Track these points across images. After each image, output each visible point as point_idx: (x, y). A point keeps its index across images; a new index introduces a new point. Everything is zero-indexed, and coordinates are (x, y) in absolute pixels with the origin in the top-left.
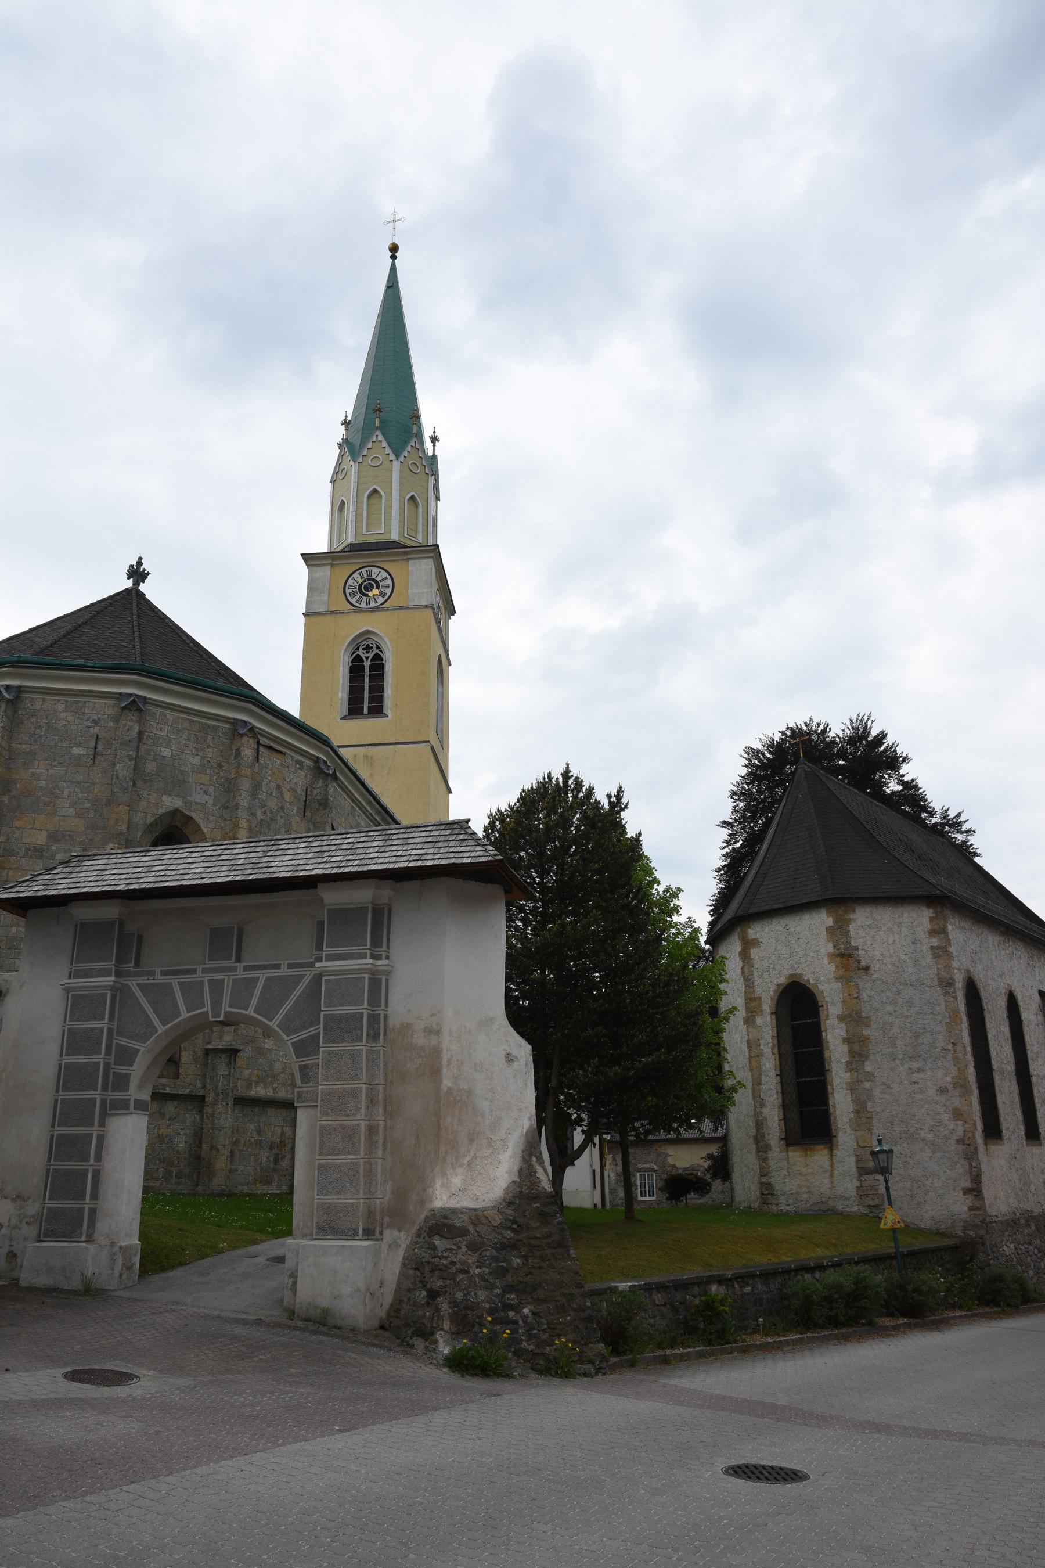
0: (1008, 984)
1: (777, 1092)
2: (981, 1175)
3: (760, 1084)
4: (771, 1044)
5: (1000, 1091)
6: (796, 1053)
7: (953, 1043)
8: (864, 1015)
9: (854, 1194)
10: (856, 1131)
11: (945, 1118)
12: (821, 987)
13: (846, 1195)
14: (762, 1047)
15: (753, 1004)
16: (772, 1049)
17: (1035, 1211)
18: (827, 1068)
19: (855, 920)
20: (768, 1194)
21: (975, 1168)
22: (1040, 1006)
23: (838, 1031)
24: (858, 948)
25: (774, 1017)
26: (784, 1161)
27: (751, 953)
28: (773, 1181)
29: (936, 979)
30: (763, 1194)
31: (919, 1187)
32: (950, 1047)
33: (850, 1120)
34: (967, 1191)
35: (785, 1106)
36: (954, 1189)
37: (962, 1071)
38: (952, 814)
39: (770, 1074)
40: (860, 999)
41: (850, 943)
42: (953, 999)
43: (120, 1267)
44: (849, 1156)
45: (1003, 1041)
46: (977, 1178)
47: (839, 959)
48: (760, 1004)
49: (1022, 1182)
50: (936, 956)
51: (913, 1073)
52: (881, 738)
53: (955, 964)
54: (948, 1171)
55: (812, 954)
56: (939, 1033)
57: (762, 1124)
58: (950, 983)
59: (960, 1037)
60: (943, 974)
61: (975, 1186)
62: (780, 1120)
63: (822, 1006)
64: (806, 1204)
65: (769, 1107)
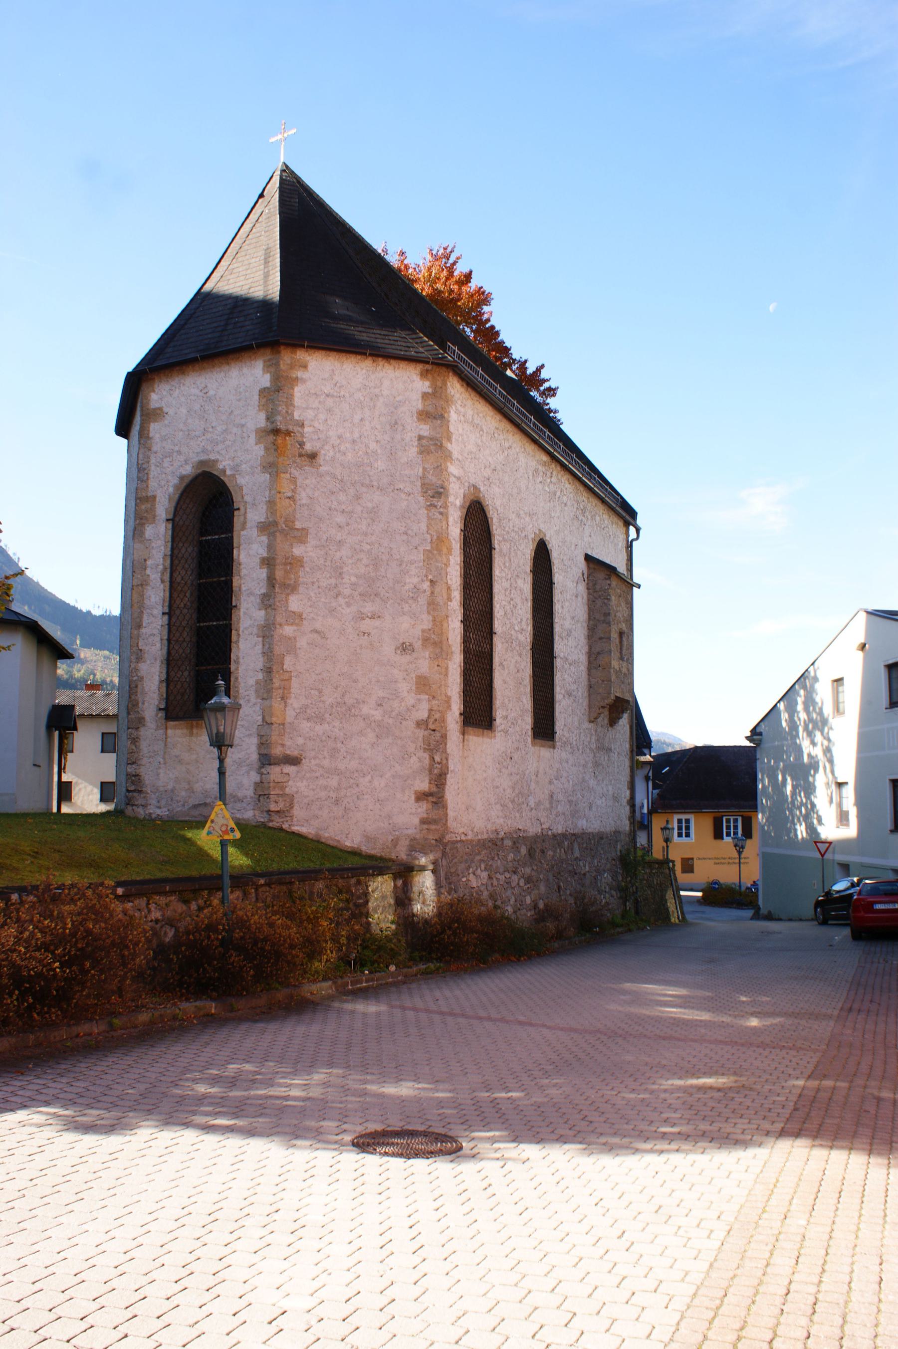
0: (539, 530)
1: (161, 640)
2: (445, 774)
3: (139, 626)
4: (161, 567)
5: (501, 664)
6: (199, 585)
7: (431, 581)
8: (298, 525)
9: (250, 792)
10: (263, 699)
11: (405, 687)
12: (241, 481)
13: (239, 794)
14: (148, 572)
15: (143, 507)
16: (163, 574)
17: (531, 830)
18: (234, 604)
19: (304, 381)
20: (134, 791)
21: (439, 763)
22: (583, 574)
23: (255, 546)
24: (303, 424)
25: (170, 526)
26: (160, 742)
27: (151, 429)
28: (143, 771)
29: (419, 484)
30: (128, 791)
31: (350, 787)
32: (426, 585)
33: (257, 682)
34: (421, 797)
35: (170, 662)
36: (403, 790)
37: (439, 623)
38: (531, 369)
39: (155, 612)
40: (294, 501)
41: (292, 415)
42: (440, 517)
43: (37, 879)
44: (250, 735)
45: (518, 600)
46: (439, 779)
47: (271, 438)
48: (153, 506)
49: (517, 791)
50: (424, 451)
51: (363, 619)
52: (468, 277)
53: (453, 469)
54: (397, 765)
55: (235, 430)
56: (412, 563)
57: (136, 686)
58: (441, 493)
59: (443, 572)
60: (432, 478)
61: (434, 789)
62: (161, 682)
63: (238, 509)
64: (184, 805)
65: (148, 662)
